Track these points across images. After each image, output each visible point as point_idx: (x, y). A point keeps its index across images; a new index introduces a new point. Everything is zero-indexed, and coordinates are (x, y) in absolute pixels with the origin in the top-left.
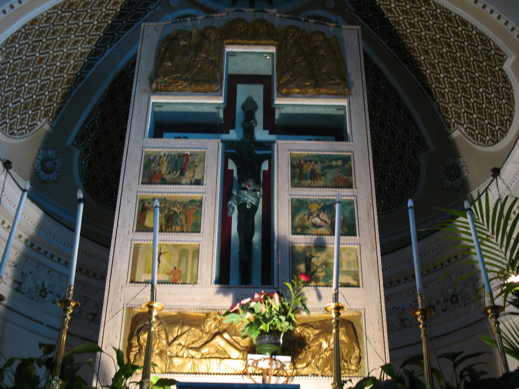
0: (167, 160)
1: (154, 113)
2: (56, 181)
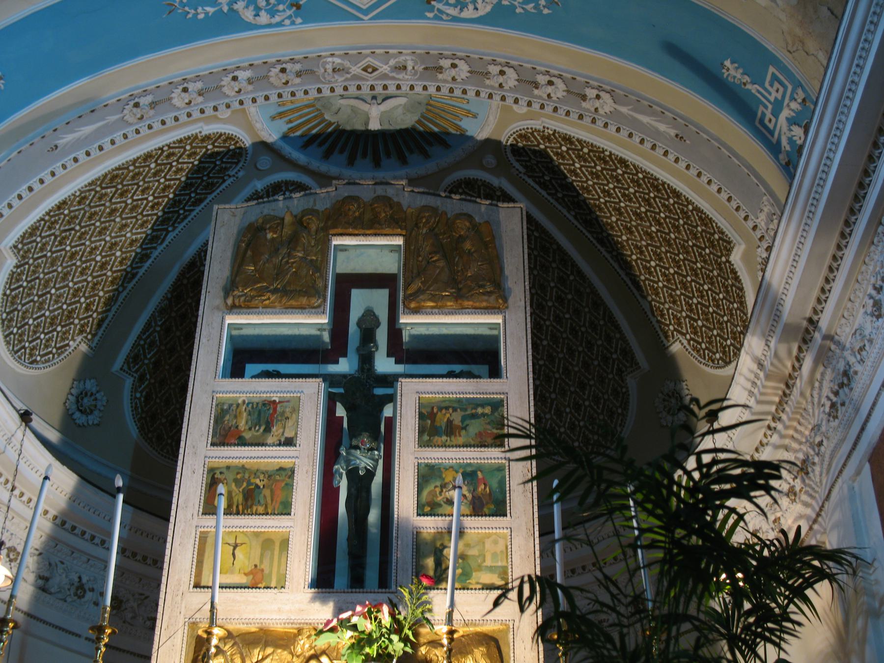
1: (231, 338)
2: (98, 425)
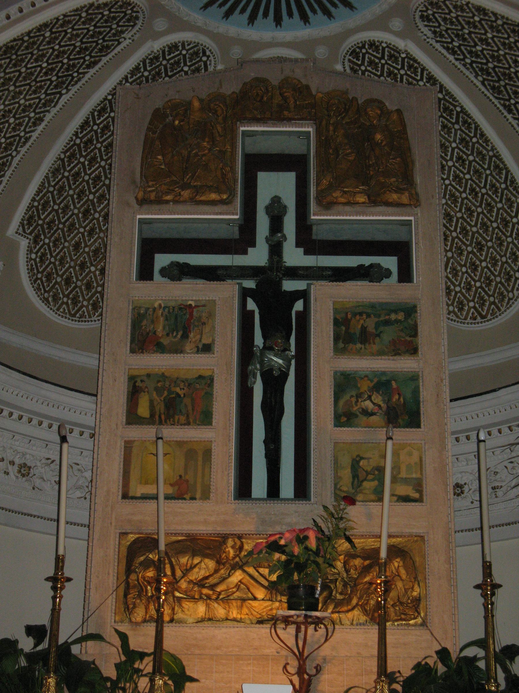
0: (164, 315)
